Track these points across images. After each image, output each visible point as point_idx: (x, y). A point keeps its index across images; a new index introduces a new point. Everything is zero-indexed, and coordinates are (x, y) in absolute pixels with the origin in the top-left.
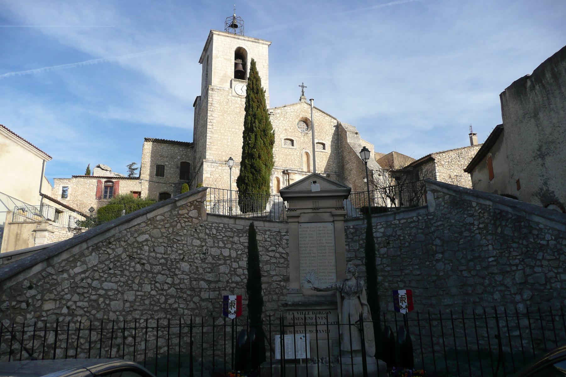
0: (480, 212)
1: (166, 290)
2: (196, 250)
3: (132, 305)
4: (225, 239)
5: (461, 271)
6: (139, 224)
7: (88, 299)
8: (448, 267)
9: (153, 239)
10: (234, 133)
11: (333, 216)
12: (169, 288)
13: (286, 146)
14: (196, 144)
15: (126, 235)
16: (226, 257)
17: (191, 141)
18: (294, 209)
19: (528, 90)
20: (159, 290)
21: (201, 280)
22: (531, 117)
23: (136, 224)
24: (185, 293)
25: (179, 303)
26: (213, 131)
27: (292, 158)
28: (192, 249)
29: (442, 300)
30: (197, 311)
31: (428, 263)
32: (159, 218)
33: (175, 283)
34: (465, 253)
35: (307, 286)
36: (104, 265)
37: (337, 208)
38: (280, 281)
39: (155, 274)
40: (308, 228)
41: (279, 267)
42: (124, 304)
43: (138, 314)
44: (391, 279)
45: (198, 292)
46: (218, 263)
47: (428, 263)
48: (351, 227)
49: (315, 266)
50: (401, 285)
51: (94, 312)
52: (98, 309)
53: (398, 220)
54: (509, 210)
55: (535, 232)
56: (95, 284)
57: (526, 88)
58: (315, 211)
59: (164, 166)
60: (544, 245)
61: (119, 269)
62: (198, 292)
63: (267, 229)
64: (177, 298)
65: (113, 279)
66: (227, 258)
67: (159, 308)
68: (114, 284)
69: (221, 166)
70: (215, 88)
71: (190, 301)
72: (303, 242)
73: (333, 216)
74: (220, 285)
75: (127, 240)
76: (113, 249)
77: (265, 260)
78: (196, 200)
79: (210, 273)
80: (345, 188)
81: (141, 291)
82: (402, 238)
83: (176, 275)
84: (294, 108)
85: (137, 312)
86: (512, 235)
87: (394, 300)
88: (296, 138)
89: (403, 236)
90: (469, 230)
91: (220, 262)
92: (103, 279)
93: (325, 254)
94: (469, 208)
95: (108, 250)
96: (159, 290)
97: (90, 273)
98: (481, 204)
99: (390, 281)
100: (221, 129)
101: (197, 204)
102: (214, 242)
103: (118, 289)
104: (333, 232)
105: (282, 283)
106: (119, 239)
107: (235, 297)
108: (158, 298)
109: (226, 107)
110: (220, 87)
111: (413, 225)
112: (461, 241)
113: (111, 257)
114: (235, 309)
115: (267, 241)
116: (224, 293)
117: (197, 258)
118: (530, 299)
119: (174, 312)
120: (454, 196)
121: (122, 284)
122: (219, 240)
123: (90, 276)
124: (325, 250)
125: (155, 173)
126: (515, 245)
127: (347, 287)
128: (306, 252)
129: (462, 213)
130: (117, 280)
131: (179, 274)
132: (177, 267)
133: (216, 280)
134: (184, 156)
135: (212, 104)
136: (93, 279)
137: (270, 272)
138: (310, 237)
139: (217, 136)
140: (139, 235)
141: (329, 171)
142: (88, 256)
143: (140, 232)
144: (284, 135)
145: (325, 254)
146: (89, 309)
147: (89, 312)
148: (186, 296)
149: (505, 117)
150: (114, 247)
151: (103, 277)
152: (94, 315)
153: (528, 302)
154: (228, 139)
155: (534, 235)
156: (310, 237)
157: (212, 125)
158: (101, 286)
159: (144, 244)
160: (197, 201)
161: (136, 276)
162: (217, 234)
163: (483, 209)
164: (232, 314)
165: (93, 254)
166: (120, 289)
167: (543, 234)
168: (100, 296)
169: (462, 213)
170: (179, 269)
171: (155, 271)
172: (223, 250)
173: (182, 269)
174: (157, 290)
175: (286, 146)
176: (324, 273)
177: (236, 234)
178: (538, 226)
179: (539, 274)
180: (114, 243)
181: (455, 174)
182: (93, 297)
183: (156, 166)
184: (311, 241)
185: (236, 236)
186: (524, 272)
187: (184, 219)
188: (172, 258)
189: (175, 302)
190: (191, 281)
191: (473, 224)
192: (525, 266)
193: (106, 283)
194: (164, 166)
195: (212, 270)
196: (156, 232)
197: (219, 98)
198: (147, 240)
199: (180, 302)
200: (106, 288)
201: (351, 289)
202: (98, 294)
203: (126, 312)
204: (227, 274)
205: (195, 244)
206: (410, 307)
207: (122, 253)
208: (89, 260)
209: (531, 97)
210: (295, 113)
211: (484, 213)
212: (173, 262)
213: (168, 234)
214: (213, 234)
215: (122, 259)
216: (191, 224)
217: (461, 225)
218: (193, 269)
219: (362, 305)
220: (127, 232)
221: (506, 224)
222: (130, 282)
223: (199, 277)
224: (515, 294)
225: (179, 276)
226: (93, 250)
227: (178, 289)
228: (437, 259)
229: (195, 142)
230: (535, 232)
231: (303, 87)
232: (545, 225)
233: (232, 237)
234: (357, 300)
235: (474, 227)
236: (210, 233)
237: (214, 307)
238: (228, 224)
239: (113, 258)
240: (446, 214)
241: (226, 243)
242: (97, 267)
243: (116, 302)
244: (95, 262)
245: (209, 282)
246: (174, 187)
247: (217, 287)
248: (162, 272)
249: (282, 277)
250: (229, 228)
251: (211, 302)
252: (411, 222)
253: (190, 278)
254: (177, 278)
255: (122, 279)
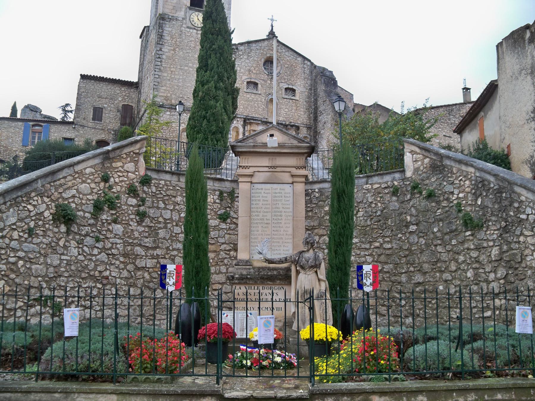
0: (461, 180)
1: (95, 255)
2: (131, 211)
3: (57, 270)
4: (166, 198)
5: (436, 246)
6: (65, 177)
7: (5, 260)
8: (422, 241)
9: (81, 196)
10: (188, 71)
11: (293, 176)
12: (100, 253)
13: (248, 91)
14: (141, 83)
15: (50, 190)
16: (167, 220)
17: (135, 80)
18: (247, 166)
19: (526, 41)
20: (88, 254)
21: (137, 246)
22: (527, 74)
23: (61, 177)
24: (117, 259)
25: (111, 271)
26: (162, 68)
27: (256, 105)
28: (127, 209)
29: (413, 278)
30: (131, 280)
31: (401, 236)
32: (88, 171)
33: (106, 247)
34: (441, 225)
35: (257, 257)
36: (24, 224)
37: (297, 168)
38: (230, 250)
39: (84, 236)
40: (262, 189)
41: (229, 234)
42: (47, 269)
43: (63, 281)
44: (358, 252)
45: (133, 259)
46: (157, 227)
47: (400, 235)
48: (317, 190)
49: (269, 235)
50: (369, 259)
51: (13, 276)
52: (18, 273)
53: (370, 184)
54: (492, 179)
55: (516, 205)
56: (14, 244)
57: (524, 41)
58: (271, 170)
59: (102, 109)
60: (523, 219)
61: (42, 229)
62: (133, 259)
63: (217, 188)
64: (109, 265)
65: (34, 239)
66: (168, 221)
67: (87, 275)
68: (35, 246)
69: (170, 111)
70: (167, 16)
71: (123, 269)
72: (255, 206)
73: (293, 176)
74: (158, 252)
75: (51, 196)
76: (34, 206)
77: (213, 225)
78: (132, 151)
79: (147, 237)
80: (308, 145)
81: (67, 255)
82: (373, 205)
83: (107, 238)
84: (260, 45)
85: (62, 278)
86: (492, 207)
87: (358, 275)
88: (261, 81)
89: (375, 204)
90: (448, 199)
91: (159, 226)
92: (23, 239)
93: (280, 221)
94: (449, 175)
95: (29, 206)
96: (88, 254)
97: (8, 232)
98: (463, 171)
99: (358, 255)
100: (172, 66)
101: (134, 155)
102: (153, 202)
103: (40, 251)
104: (291, 195)
105: (232, 253)
106: (42, 193)
107: (174, 266)
108: (86, 263)
109: (178, 40)
110: (172, 16)
111: (387, 192)
112: (438, 211)
113: (32, 214)
114: (174, 281)
115: (217, 203)
116: (163, 262)
117: (132, 220)
118: (503, 278)
119: (105, 282)
120: (435, 160)
121: (45, 246)
122: (159, 199)
123: (8, 236)
124: (281, 216)
125: (92, 117)
126: (493, 218)
127: (303, 259)
128: (259, 218)
129: (441, 179)
130: (39, 241)
131: (110, 238)
132: (109, 229)
133: (154, 246)
134: (126, 98)
135: (161, 36)
136: (12, 239)
137: (219, 239)
138: (263, 200)
139: (166, 75)
140: (65, 190)
141: (299, 122)
142: (5, 212)
143: (65, 187)
144: (246, 77)
145: (280, 221)
146: (8, 273)
147: (7, 276)
148: (119, 263)
149: (501, 72)
150: (35, 203)
151: (23, 237)
152: (13, 280)
153: (502, 281)
154: (179, 79)
155: (514, 207)
156: (263, 200)
157: (161, 62)
158: (20, 246)
159: (70, 200)
160: (134, 153)
161: (61, 238)
162: (157, 192)
163: (465, 176)
164: (171, 286)
165: (11, 210)
166: (43, 252)
167: (524, 207)
168: (20, 258)
169: (441, 179)
170: (111, 232)
171: (83, 232)
172: (163, 212)
173: (114, 232)
174: (85, 254)
175: (248, 91)
176: (279, 242)
177: (179, 193)
178: (519, 199)
179: (515, 251)
180: (36, 198)
181: (444, 134)
182: (12, 260)
183: (92, 108)
184: (265, 204)
185: (179, 196)
186: (501, 249)
187: (118, 174)
188: (103, 218)
189: (106, 269)
190: (125, 246)
191: (452, 193)
192: (502, 241)
193: (26, 244)
194: (102, 109)
195: (149, 235)
196: (83, 187)
197: (170, 29)
198: (74, 196)
199: (111, 270)
200: (26, 249)
201: (308, 262)
202: (17, 257)
203: (49, 278)
204: (167, 240)
205: (130, 203)
206: (375, 284)
207: (45, 210)
208: (7, 216)
209: (529, 51)
210: (262, 52)
211: (465, 181)
212: (104, 223)
213: (99, 191)
214: (152, 192)
215: (45, 218)
216: (126, 179)
217: (440, 194)
218: (127, 233)
219: (319, 280)
220: (51, 186)
221: (486, 194)
222: (53, 244)
223: (135, 242)
224: (489, 272)
225: (111, 240)
226: (11, 205)
227: (110, 255)
228: (411, 232)
229: (140, 82)
230: (516, 205)
231: (272, 20)
232: (526, 197)
233: (175, 197)
234: (315, 274)
235: (453, 197)
236: (148, 191)
237: (151, 277)
238: (170, 181)
239: (35, 215)
240: (424, 180)
241: (167, 203)
242: (16, 225)
243: (38, 266)
244: (13, 220)
245: (147, 248)
246: (113, 134)
247: (155, 255)
248: (91, 235)
249: (232, 245)
250: (171, 186)
251: (148, 271)
252: (386, 188)
253: (124, 242)
254: (109, 241)
255: (44, 240)
